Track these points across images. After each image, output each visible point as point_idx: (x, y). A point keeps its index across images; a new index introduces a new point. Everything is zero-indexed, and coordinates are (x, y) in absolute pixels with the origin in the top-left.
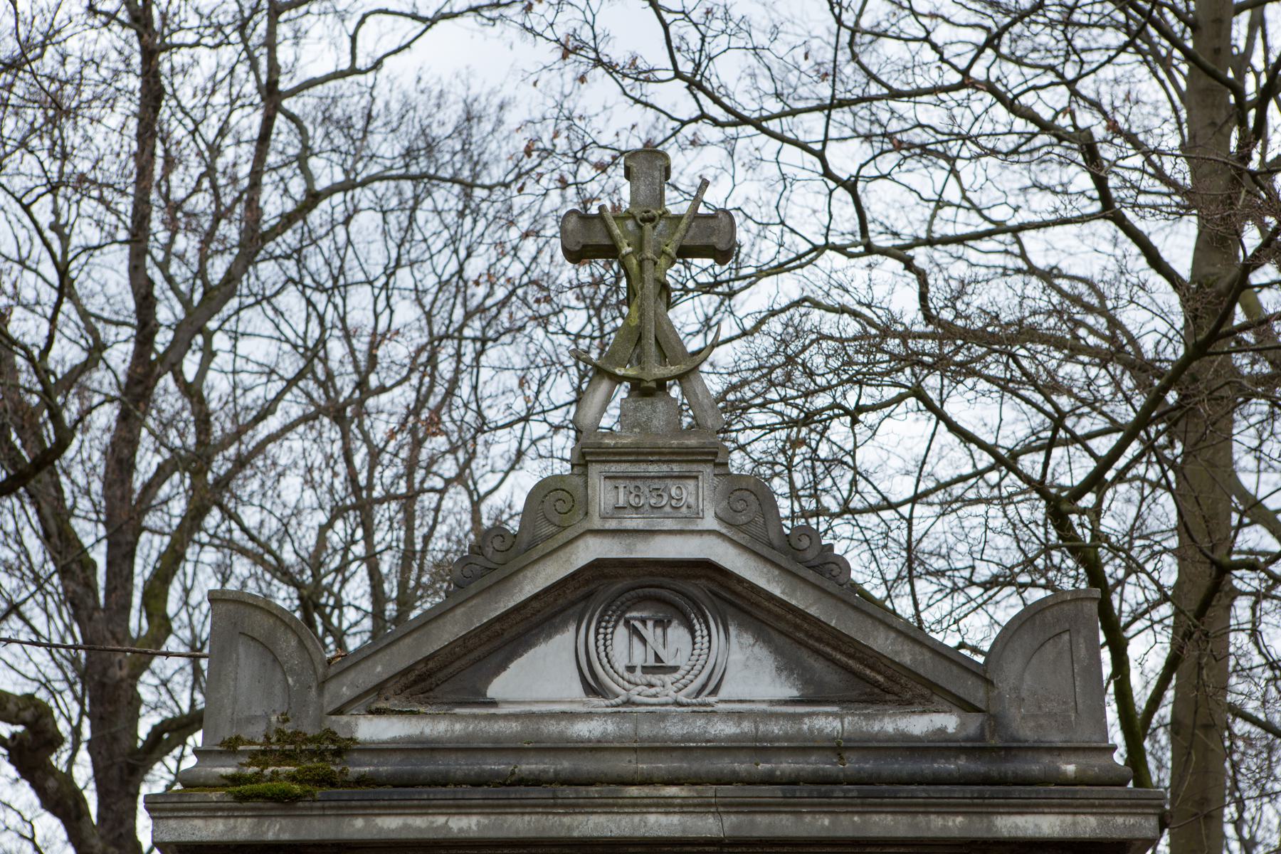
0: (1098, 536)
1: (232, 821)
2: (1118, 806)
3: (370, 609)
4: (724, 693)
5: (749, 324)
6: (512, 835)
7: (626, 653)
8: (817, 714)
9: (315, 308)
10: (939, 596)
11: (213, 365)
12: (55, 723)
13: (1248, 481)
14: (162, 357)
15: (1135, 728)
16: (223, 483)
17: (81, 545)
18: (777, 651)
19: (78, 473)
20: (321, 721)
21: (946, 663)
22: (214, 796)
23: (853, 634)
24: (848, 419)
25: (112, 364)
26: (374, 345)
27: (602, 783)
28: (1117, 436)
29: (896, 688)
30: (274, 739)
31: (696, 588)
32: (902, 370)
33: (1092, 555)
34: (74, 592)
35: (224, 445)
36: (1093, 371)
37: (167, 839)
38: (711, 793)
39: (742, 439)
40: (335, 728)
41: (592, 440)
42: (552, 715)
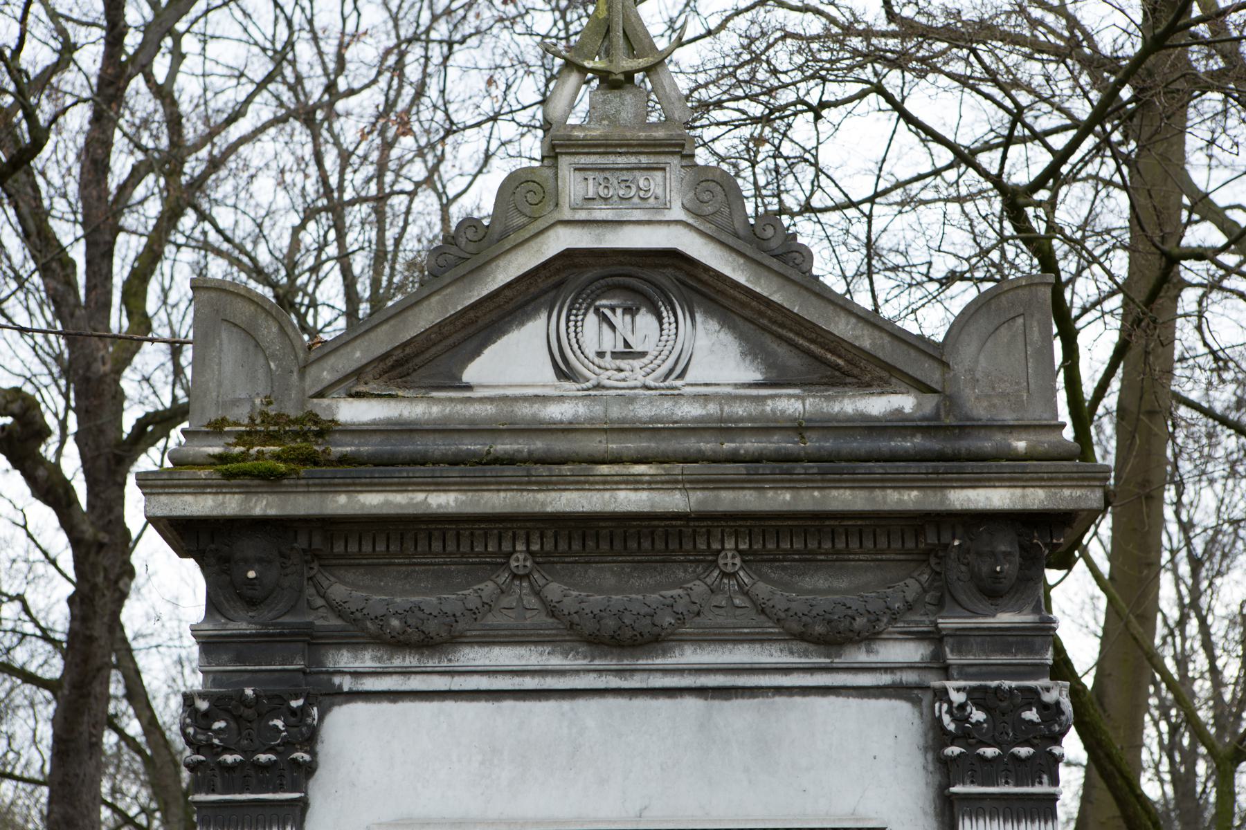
0: (1053, 228)
1: (220, 497)
2: (1065, 479)
3: (344, 309)
4: (689, 378)
5: (713, 23)
6: (489, 510)
7: (596, 339)
8: (780, 396)
9: (282, 10)
10: (896, 291)
11: (182, 68)
12: (42, 416)
13: (1199, 177)
14: (132, 59)
15: (1082, 414)
16: (198, 183)
17: (60, 245)
18: (741, 336)
19: (54, 175)
20: (302, 404)
21: (905, 347)
22: (203, 473)
23: (814, 320)
24: (810, 115)
25: (84, 67)
26: (342, 46)
27: (574, 462)
28: (1072, 133)
29: (856, 371)
30: (258, 421)
31: (664, 277)
32: (862, 67)
33: (1046, 247)
34: (55, 289)
35: (197, 147)
36: (1051, 67)
37: (159, 513)
38: (678, 471)
39: (708, 134)
40: (317, 411)
41: (561, 132)
42: (525, 398)
